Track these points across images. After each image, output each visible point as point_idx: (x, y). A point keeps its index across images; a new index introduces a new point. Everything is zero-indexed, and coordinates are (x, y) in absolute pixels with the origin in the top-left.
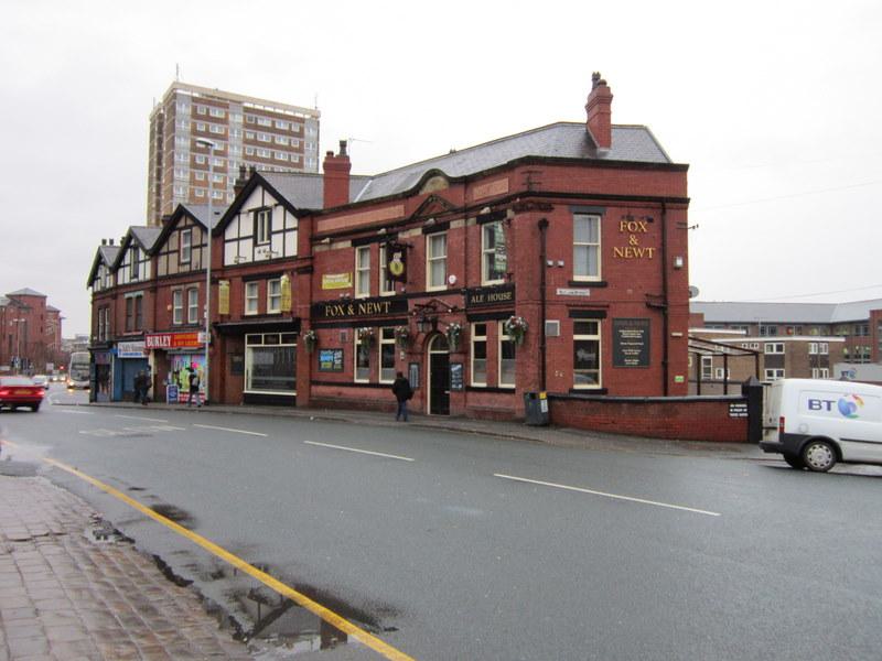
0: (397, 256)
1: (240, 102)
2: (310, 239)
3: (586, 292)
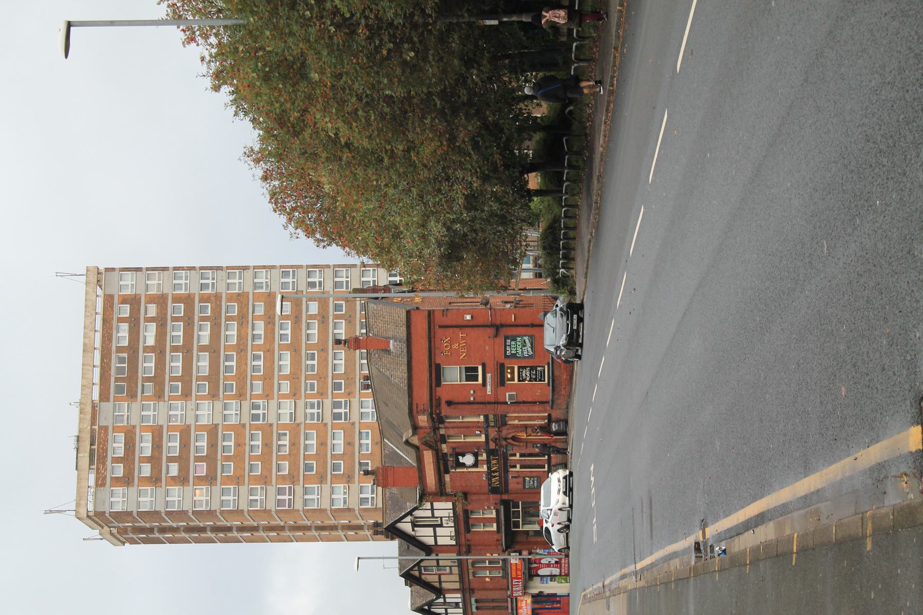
0: (461, 460)
1: (94, 407)
2: (441, 493)
3: (489, 375)
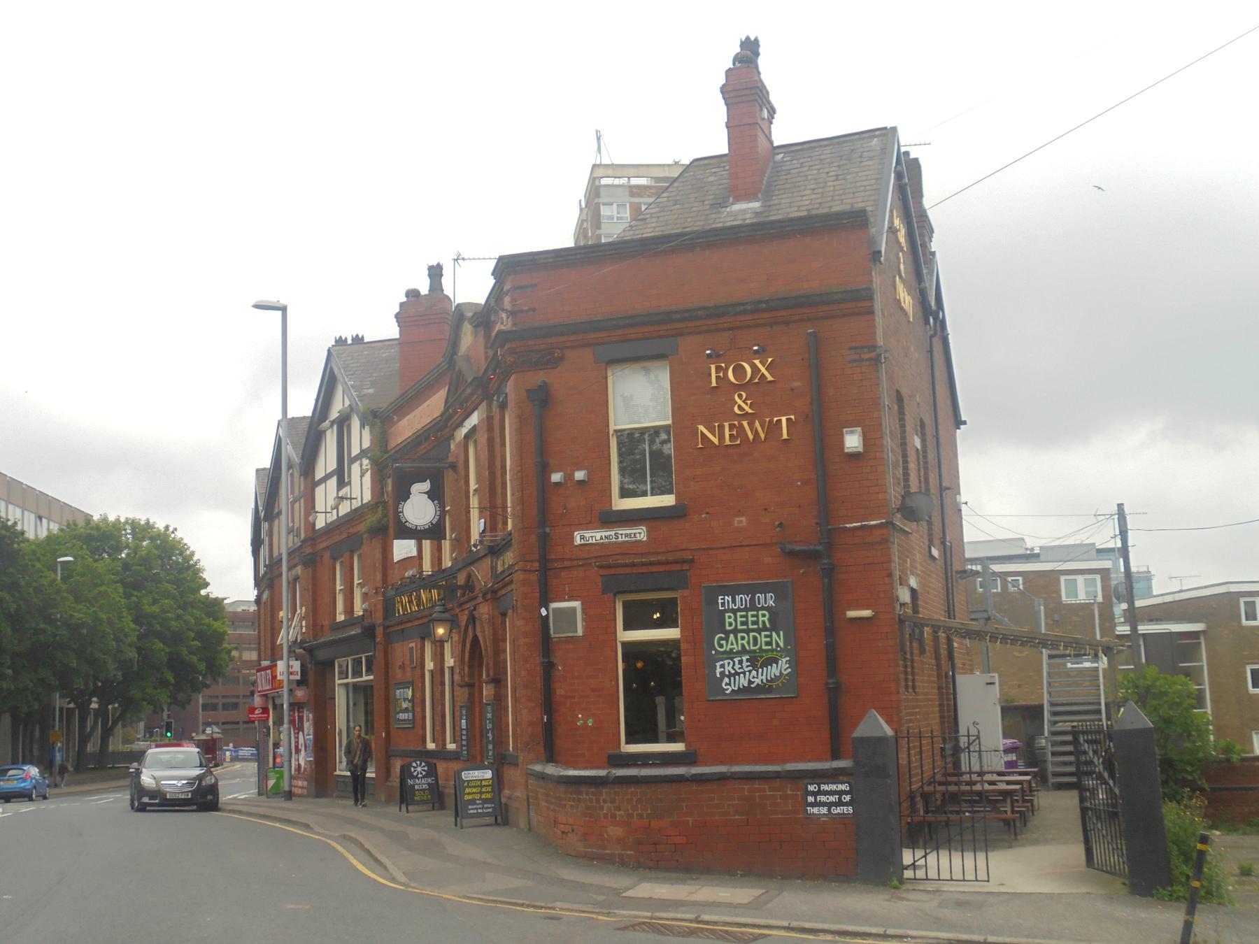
0: (419, 490)
3: (640, 533)
